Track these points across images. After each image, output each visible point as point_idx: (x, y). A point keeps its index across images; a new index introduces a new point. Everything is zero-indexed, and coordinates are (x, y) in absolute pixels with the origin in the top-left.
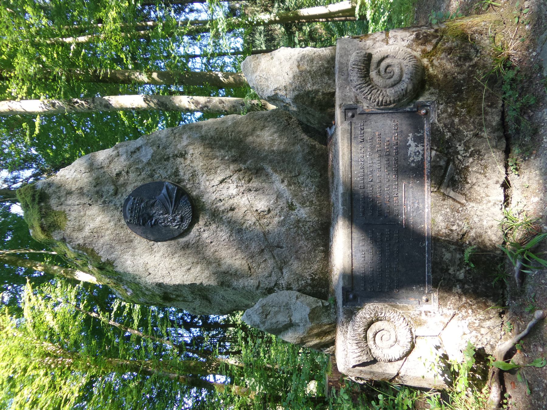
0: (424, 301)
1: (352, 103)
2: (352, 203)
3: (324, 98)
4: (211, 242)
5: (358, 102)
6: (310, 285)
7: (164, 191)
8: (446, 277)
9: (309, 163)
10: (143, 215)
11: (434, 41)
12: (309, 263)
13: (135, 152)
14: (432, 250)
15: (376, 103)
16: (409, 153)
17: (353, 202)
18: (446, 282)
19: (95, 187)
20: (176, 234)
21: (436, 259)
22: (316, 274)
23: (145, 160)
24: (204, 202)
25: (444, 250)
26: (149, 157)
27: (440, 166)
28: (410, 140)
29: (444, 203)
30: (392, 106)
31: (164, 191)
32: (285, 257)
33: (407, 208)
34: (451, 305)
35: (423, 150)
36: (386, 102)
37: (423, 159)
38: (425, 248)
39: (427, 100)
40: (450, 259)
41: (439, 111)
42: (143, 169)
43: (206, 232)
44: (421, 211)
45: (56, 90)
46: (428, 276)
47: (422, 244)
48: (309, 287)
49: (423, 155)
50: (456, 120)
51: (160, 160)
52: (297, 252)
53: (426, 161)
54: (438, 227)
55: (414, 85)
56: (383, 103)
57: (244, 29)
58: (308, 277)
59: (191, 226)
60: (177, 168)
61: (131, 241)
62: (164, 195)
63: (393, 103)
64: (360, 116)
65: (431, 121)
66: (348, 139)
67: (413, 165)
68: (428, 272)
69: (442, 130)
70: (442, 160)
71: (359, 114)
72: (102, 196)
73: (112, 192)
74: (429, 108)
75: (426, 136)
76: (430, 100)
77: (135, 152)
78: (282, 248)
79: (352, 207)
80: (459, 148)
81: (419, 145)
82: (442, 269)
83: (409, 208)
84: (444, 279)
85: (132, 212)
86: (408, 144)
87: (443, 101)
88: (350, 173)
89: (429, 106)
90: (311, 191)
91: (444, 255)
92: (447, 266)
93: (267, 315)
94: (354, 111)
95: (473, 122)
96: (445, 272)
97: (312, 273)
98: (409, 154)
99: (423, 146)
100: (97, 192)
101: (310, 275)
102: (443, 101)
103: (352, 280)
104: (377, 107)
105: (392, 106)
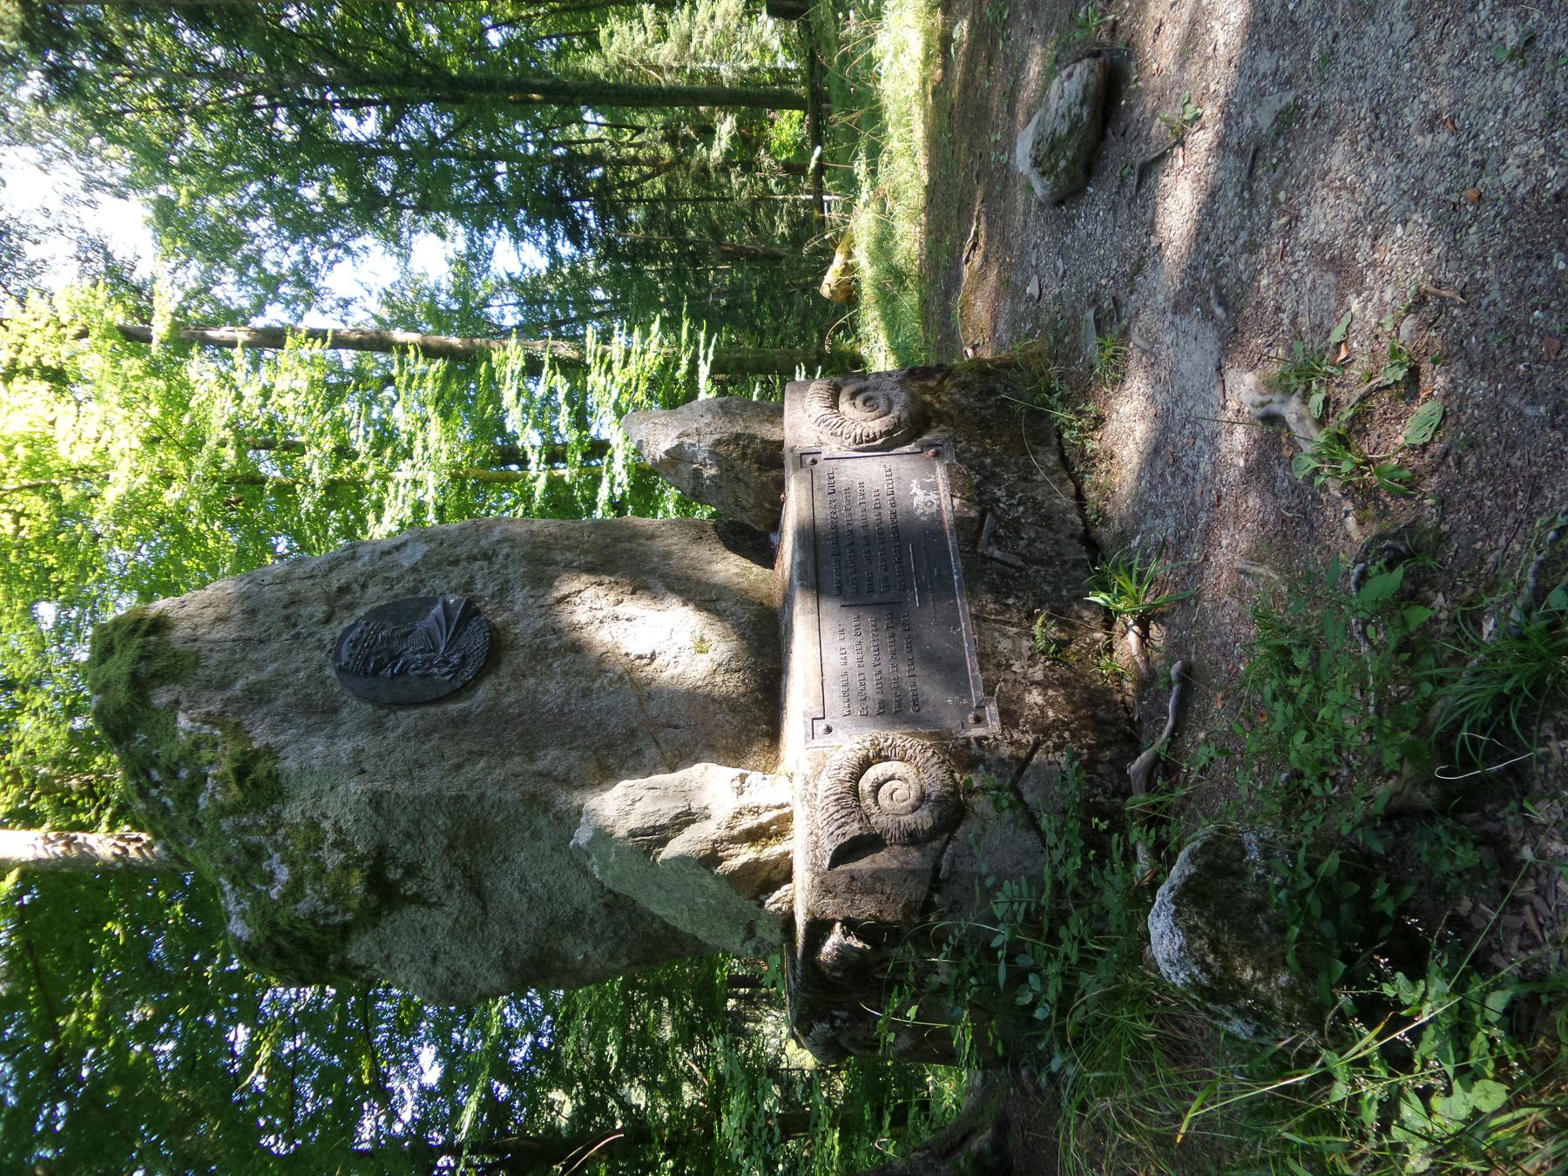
0: (971, 721)
3: (764, 449)
4: (519, 715)
7: (437, 609)
10: (378, 653)
11: (938, 376)
13: (389, 553)
19: (285, 607)
20: (446, 690)
23: (406, 564)
25: (996, 634)
26: (419, 557)
30: (879, 442)
31: (437, 609)
32: (684, 745)
42: (400, 579)
43: (513, 692)
45: (97, 800)
50: (988, 461)
51: (440, 563)
52: (708, 734)
55: (911, 416)
59: (480, 675)
60: (472, 577)
61: (335, 711)
62: (437, 619)
72: (295, 626)
73: (320, 616)
75: (940, 481)
77: (389, 553)
78: (676, 727)
80: (999, 493)
82: (998, 665)
85: (355, 647)
93: (634, 802)
95: (1016, 463)
100: (288, 618)
103: (816, 549)
105: (879, 442)
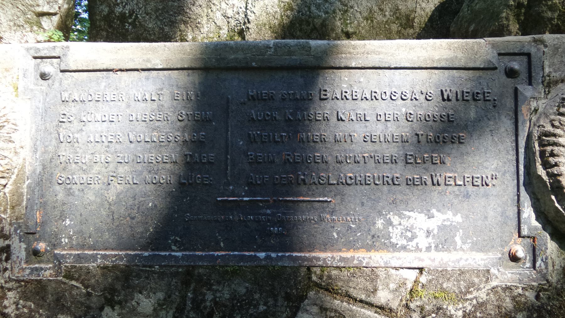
1: (547, 70)
2: (282, 68)
5: (549, 85)
6: (111, 12)
8: (94, 299)
9: (375, 8)
12: (157, 10)
14: (160, 266)
15: (549, 128)
16: (411, 214)
17: (285, 74)
18: (82, 300)
21: (138, 276)
22: (134, 26)
24: (322, 220)
25: (161, 295)
27: (375, 290)
28: (445, 217)
29: (280, 299)
30: (541, 171)
33: (268, 208)
34: (26, 310)
35: (418, 249)
36: (552, 155)
37: (394, 247)
38: (165, 250)
39: (550, 261)
40: (139, 309)
41: (520, 291)
44: (259, 241)
46: (94, 257)
47: (175, 242)
48: (106, 10)
49: (404, 248)
53: (389, 255)
54: (219, 283)
56: (549, 149)
57: (539, 14)
58: (128, 7)
63: (548, 174)
64: (511, 91)
65: (493, 271)
66: (452, 59)
67: (380, 223)
68: (104, 257)
69: (469, 296)
70: (390, 296)
71: (516, 90)
74: (528, 265)
76: (550, 268)
79: (271, 69)
81: (430, 240)
83: (269, 211)
84: (89, 294)
86: (434, 211)
87: (545, 301)
88: (360, 64)
89: (534, 267)
90: (313, 8)
91: (148, 297)
92: (120, 303)
94: (524, 76)
96: (106, 298)
97: (137, 17)
98: (407, 213)
99: (428, 249)
101: (132, 12)
102: (545, 301)
104: (536, 134)
105: (541, 171)
